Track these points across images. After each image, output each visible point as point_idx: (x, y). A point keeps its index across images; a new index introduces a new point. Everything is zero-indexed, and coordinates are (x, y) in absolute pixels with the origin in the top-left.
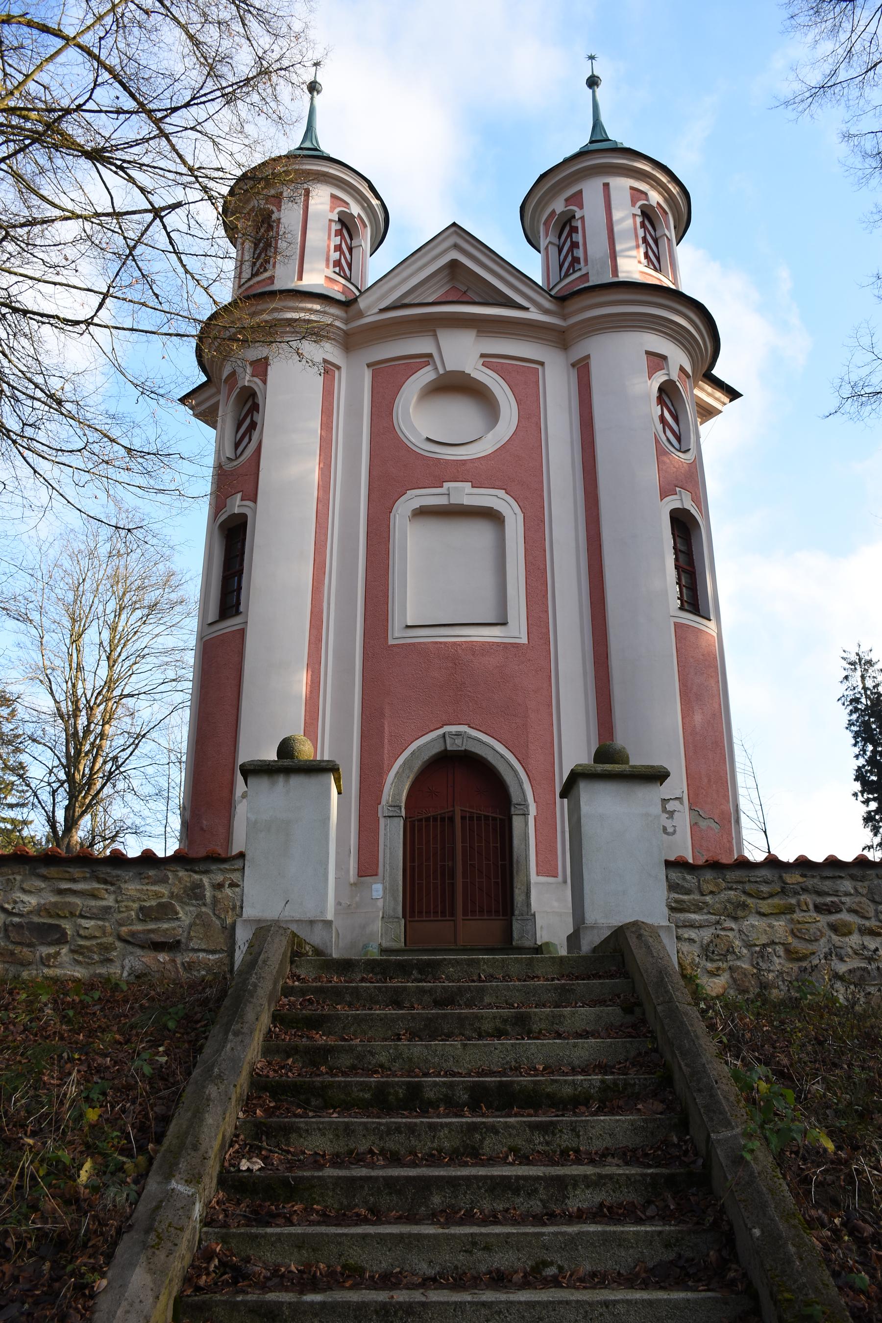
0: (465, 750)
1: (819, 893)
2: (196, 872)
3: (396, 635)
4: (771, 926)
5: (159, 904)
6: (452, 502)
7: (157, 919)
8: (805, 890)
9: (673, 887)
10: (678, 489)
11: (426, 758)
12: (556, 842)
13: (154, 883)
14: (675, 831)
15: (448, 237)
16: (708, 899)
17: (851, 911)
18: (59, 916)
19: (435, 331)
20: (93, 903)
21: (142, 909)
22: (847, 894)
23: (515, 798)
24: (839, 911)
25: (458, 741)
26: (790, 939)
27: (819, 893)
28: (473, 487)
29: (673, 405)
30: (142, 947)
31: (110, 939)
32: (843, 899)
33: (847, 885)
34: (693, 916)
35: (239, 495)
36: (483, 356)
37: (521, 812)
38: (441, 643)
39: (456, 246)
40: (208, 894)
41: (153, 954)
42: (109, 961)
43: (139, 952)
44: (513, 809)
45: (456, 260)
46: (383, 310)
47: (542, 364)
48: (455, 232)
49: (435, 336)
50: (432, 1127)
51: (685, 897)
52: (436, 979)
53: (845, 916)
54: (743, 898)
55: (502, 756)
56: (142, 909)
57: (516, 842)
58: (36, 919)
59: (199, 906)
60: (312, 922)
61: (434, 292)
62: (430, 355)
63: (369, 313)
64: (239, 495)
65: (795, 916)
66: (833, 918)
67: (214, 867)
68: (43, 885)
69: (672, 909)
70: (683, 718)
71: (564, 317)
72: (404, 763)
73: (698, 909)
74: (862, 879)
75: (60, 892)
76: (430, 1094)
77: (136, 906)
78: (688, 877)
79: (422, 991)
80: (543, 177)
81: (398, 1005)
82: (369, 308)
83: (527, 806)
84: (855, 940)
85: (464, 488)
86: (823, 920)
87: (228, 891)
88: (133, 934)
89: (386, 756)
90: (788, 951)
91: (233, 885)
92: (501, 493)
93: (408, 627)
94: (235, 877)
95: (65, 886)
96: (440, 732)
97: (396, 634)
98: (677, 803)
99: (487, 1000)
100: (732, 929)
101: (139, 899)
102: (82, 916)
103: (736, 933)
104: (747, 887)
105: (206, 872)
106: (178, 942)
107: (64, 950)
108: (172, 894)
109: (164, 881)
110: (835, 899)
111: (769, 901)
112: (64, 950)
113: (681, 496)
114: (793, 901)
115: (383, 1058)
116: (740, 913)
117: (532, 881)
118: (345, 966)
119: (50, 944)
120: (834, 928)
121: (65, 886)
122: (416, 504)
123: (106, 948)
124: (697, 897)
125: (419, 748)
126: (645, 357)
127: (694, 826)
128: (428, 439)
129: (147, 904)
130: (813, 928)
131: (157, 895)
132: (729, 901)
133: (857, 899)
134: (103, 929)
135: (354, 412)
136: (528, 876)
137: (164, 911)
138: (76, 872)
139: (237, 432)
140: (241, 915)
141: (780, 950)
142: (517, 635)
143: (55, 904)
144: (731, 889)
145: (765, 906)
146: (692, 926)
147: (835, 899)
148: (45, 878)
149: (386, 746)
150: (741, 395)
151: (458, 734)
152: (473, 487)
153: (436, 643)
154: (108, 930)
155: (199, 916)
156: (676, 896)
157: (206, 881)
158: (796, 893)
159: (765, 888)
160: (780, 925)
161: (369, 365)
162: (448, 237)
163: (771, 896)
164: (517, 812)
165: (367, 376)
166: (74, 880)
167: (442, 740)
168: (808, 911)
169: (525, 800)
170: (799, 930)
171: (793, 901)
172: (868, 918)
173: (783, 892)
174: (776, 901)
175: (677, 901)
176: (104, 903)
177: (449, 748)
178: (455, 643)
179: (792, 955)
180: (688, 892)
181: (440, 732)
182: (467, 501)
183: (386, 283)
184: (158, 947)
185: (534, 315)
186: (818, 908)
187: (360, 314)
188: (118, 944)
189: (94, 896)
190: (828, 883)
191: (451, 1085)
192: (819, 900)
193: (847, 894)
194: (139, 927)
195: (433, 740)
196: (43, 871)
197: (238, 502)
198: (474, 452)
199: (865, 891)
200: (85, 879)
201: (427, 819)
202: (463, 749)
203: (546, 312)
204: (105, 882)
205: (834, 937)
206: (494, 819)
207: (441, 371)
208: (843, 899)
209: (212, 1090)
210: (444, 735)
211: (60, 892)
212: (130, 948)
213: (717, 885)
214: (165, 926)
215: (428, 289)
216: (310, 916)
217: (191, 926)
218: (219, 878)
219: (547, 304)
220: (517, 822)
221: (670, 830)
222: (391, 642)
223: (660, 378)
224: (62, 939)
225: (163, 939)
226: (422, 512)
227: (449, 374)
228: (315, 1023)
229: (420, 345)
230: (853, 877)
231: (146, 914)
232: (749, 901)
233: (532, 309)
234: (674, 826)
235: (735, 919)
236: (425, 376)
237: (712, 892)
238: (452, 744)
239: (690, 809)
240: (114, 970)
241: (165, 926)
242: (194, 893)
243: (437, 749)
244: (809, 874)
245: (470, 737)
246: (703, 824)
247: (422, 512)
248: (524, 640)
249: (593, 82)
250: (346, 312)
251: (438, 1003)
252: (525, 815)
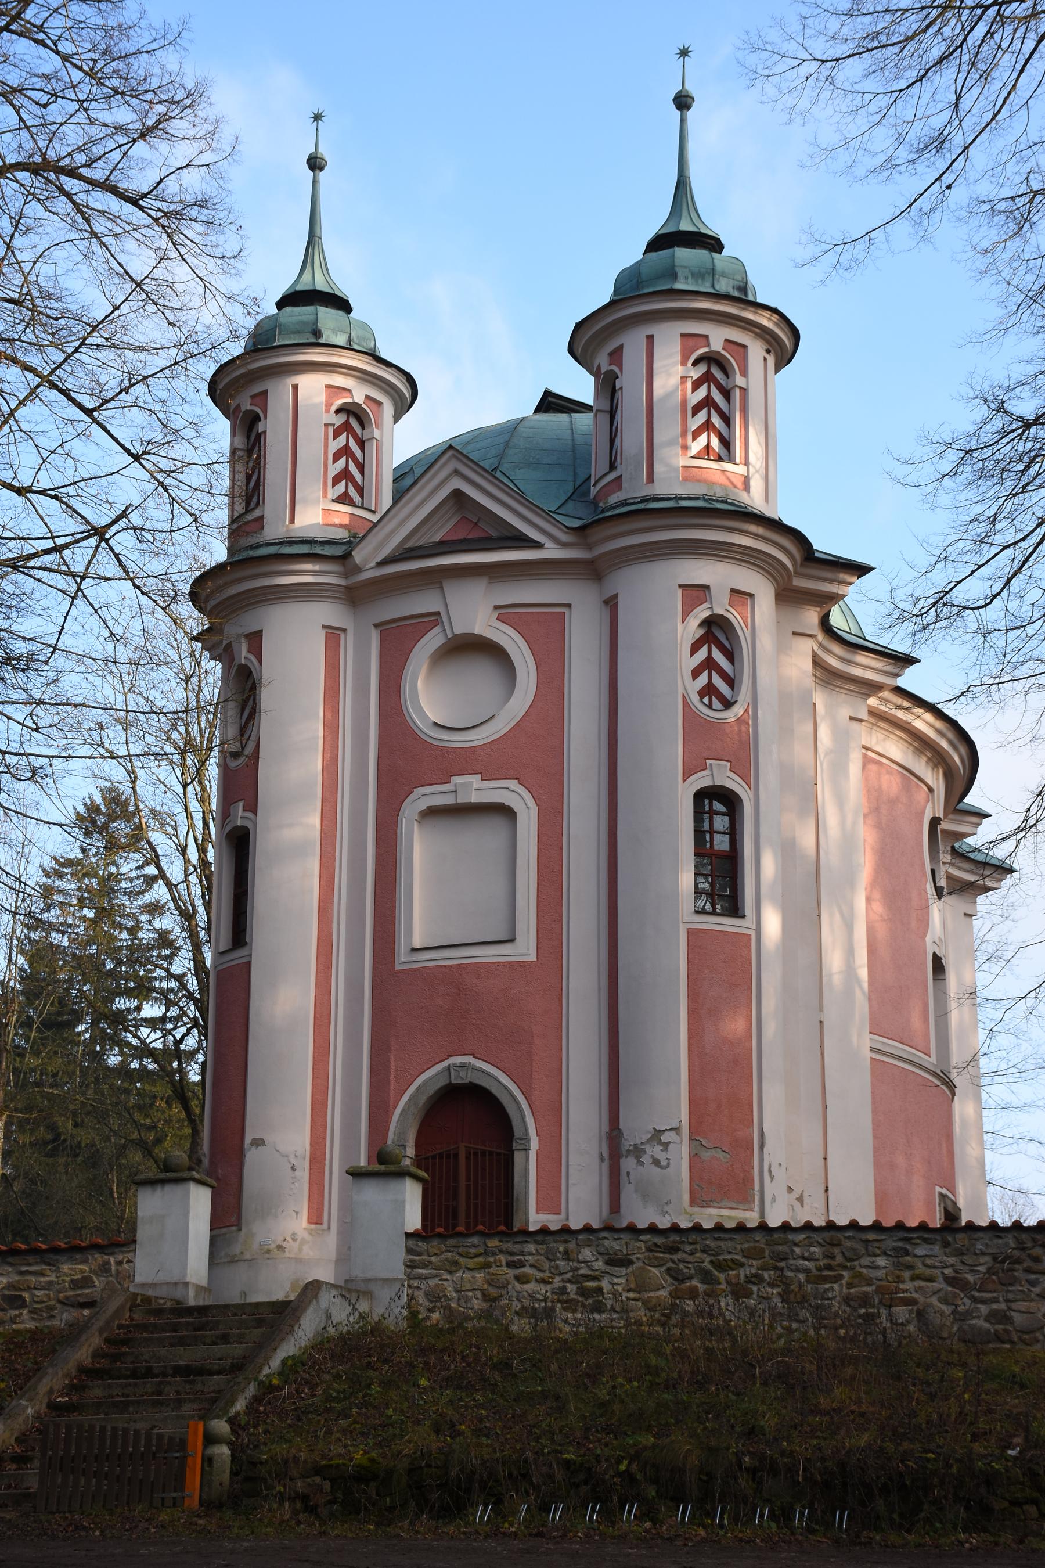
0: (471, 1083)
1: (512, 1254)
2: (106, 1254)
3: (403, 959)
4: (474, 1277)
5: (83, 1277)
6: (459, 801)
7: (82, 1287)
8: (501, 1251)
9: (409, 1251)
10: (708, 762)
11: (431, 1092)
12: (560, 1177)
13: (80, 1263)
14: (669, 1164)
15: (445, 464)
16: (433, 1259)
17: (532, 1266)
18: (21, 1290)
19: (441, 582)
20: (42, 1279)
21: (72, 1281)
22: (530, 1254)
23: (518, 1132)
24: (524, 1266)
25: (462, 1074)
26: (486, 1287)
27: (512, 1254)
28: (482, 780)
29: (727, 638)
30: (73, 1306)
31: (52, 1303)
32: (527, 1258)
33: (531, 1247)
34: (421, 1271)
35: (241, 804)
36: (496, 607)
37: (522, 1147)
38: (445, 966)
39: (456, 472)
40: (113, 1268)
41: (80, 1310)
42: (53, 1317)
43: (72, 1310)
44: (514, 1144)
45: (458, 490)
46: (381, 564)
47: (569, 606)
48: (454, 456)
49: (442, 587)
50: (145, 1383)
51: (417, 1258)
52: (207, 1316)
53: (527, 1270)
54: (457, 1257)
55: (506, 1088)
56: (72, 1281)
57: (517, 1179)
58: (7, 1293)
59: (107, 1277)
60: (176, 1284)
61: (441, 527)
62: (438, 613)
63: (367, 567)
64: (241, 804)
65: (492, 1270)
66: (518, 1271)
67: (117, 1250)
68: (10, 1269)
69: (407, 1266)
70: (689, 1038)
71: (589, 547)
72: (410, 1100)
73: (425, 1266)
74: (543, 1243)
75: (22, 1273)
76: (156, 1371)
77: (68, 1279)
78: (420, 1244)
79: (188, 1323)
80: (579, 326)
81: (175, 1331)
82: (366, 561)
83: (528, 1140)
84: (531, 1287)
85: (472, 783)
86: (511, 1273)
87: (126, 1266)
88: (67, 1298)
89: (392, 1093)
90: (484, 1295)
91: (129, 1261)
92: (513, 784)
93: (414, 950)
94: (130, 1256)
95: (24, 1269)
96: (445, 1064)
97: (403, 958)
98: (673, 1134)
99: (221, 1327)
100: (447, 1280)
101: (71, 1275)
102: (35, 1288)
103: (450, 1283)
104: (460, 1250)
105: (112, 1254)
106: (95, 1301)
107: (25, 1312)
108: (91, 1271)
109: (85, 1261)
110: (521, 1258)
111: (476, 1260)
112: (25, 1312)
113: (712, 770)
114: (492, 1259)
115: (146, 1357)
116: (453, 1269)
117: (531, 1220)
118: (159, 1312)
119: (16, 1308)
120: (517, 1278)
121: (24, 1269)
122: (423, 804)
123: (51, 1308)
124: (425, 1257)
125: (425, 1083)
126: (679, 592)
127: (694, 1157)
128: (435, 724)
129: (75, 1278)
130: (502, 1278)
131: (82, 1271)
132: (447, 1260)
133: (539, 1257)
134: (48, 1296)
135: (361, 690)
136: (527, 1214)
137: (85, 1282)
138: (31, 1259)
139: (241, 718)
140: (133, 1281)
141: (479, 1294)
142: (524, 952)
143: (18, 1282)
144: (449, 1251)
145: (471, 1263)
146: (420, 1277)
147: (521, 1258)
148: (11, 1265)
149: (392, 1082)
150: (872, 569)
151: (463, 1066)
152: (482, 780)
153: (441, 966)
154: (52, 1296)
155: (108, 1283)
156: (411, 1257)
157: (112, 1260)
158: (494, 1254)
159: (472, 1251)
160: (480, 1275)
161: (376, 626)
162: (445, 464)
163: (476, 1256)
164: (518, 1147)
165: (375, 637)
166: (30, 1265)
167: (446, 1073)
168: (501, 1266)
169: (527, 1133)
170: (492, 1280)
171: (492, 1259)
172: (544, 1271)
173: (485, 1253)
174: (481, 1259)
175: (411, 1261)
176: (48, 1279)
177: (453, 1082)
178: (459, 966)
179: (486, 1297)
180: (420, 1254)
181: (445, 1064)
182: (475, 798)
183: (383, 528)
184: (83, 1305)
185: (551, 552)
186: (509, 1265)
187: (358, 570)
188: (58, 1305)
189: (43, 1275)
190: (517, 1246)
191: (165, 1367)
192: (510, 1258)
193: (530, 1254)
194: (71, 1293)
195: (439, 1073)
196: (10, 1260)
197: (240, 813)
198: (485, 735)
199: (542, 1252)
200: (37, 1263)
201: (441, 1155)
202: (467, 1081)
203: (564, 545)
204: (49, 1264)
205: (517, 1284)
206: (498, 1154)
207: (450, 636)
208: (527, 1258)
209: (50, 1370)
210: (449, 1068)
211: (22, 1273)
212: (66, 1308)
213: (439, 1249)
214: (87, 1291)
215: (433, 526)
216: (176, 1279)
217: (102, 1290)
218: (120, 1257)
219: (564, 537)
220: (518, 1157)
221: (664, 1163)
222: (398, 967)
223: (703, 613)
224: (23, 1304)
225: (86, 1300)
226: (432, 813)
227: (456, 636)
228: (125, 1342)
229: (423, 603)
230: (536, 1242)
231: (75, 1284)
232: (462, 1260)
233: (548, 544)
234: (669, 1159)
235: (450, 1272)
236: (433, 641)
237: (436, 1254)
238: (458, 1076)
239: (691, 1139)
240: (56, 1322)
241: (87, 1291)
242: (105, 1268)
243: (442, 1082)
244: (505, 1239)
245: (476, 1069)
246: (706, 1155)
247: (432, 813)
248: (533, 957)
249: (683, 102)
250: (344, 565)
251: (195, 1330)
252: (527, 1150)
